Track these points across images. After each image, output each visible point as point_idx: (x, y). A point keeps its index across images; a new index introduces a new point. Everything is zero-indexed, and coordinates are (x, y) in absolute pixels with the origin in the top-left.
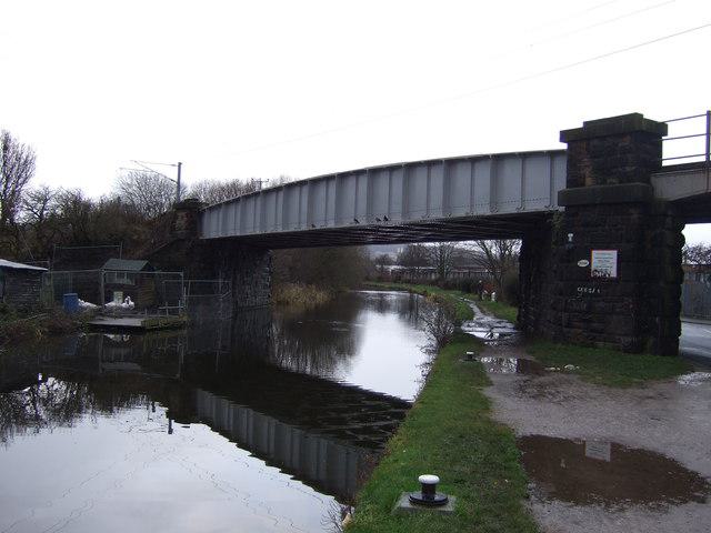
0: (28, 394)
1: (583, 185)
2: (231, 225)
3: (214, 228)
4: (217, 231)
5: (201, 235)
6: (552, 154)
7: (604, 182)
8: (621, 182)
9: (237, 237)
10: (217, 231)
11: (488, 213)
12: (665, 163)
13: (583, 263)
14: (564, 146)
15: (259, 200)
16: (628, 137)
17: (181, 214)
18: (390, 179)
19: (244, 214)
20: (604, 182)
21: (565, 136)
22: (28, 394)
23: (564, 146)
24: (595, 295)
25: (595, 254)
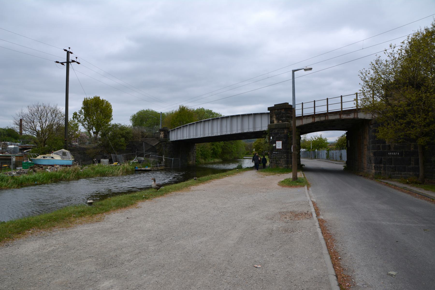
0: (422, 119)
1: (274, 123)
2: (192, 134)
3: (173, 137)
4: (209, 134)
5: (169, 140)
6: (268, 113)
7: (279, 122)
8: (282, 122)
9: (194, 139)
10: (209, 134)
11: (252, 131)
12: (296, 116)
13: (274, 145)
14: (269, 112)
15: (219, 121)
16: (283, 110)
17: (162, 133)
18: (217, 123)
19: (196, 129)
20: (279, 122)
21: (269, 109)
22: (422, 119)
23: (269, 112)
24: (277, 154)
25: (277, 142)
